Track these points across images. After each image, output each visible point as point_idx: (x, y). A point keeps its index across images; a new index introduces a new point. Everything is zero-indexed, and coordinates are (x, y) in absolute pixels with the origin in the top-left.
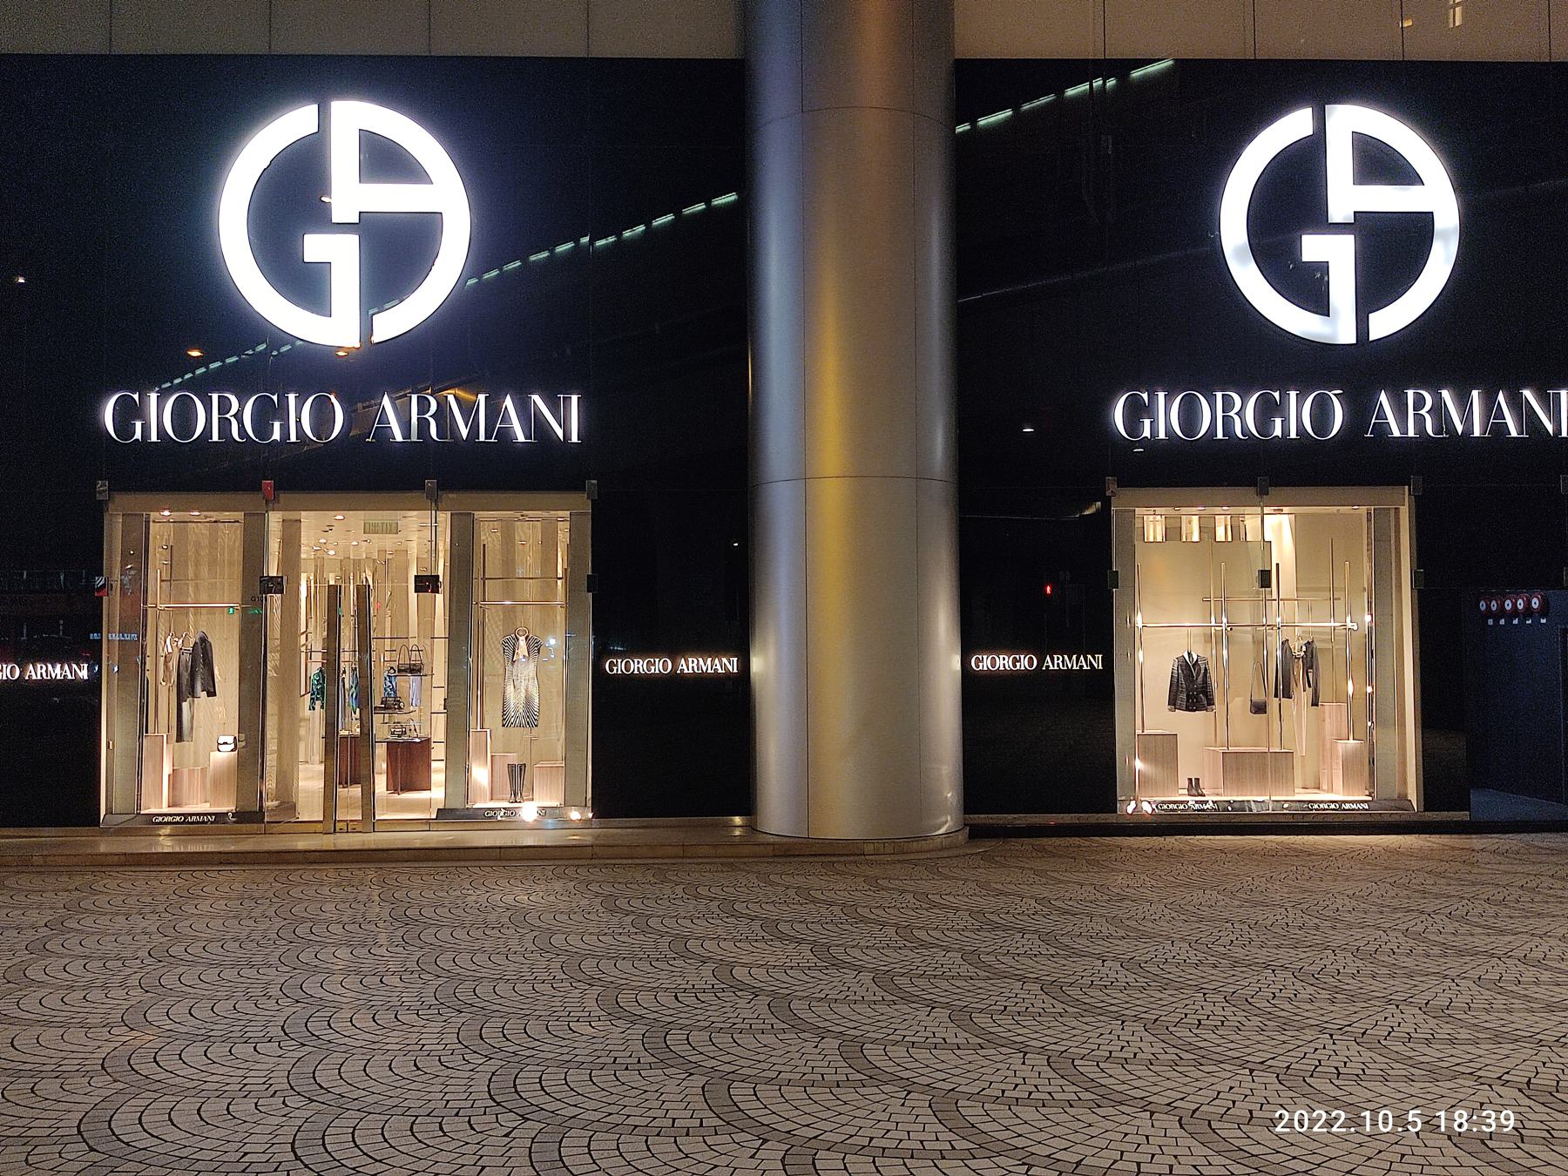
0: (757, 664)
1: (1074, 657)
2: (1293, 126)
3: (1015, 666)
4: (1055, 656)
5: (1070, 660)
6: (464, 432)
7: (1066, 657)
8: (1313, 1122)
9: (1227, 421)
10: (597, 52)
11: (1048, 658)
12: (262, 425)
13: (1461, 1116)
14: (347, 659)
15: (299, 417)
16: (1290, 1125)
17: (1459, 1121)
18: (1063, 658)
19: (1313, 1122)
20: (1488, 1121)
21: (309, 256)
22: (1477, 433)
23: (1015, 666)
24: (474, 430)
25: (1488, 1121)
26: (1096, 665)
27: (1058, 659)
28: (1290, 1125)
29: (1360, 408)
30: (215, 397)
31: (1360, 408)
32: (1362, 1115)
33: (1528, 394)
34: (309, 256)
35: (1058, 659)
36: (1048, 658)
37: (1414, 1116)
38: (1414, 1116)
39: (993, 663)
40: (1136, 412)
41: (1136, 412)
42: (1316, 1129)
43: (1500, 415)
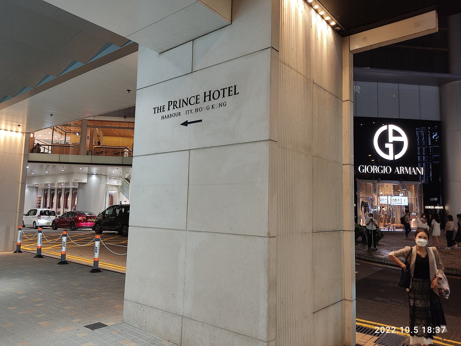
1: (410, 168)
2: (384, 128)
3: (380, 171)
4: (401, 167)
5: (408, 169)
7: (406, 168)
9: (375, 170)
10: (422, 118)
11: (397, 168)
13: (429, 328)
14: (48, 199)
15: (385, 170)
17: (430, 330)
20: (437, 330)
21: (386, 147)
22: (410, 174)
23: (380, 171)
24: (421, 174)
25: (437, 330)
26: (420, 173)
27: (402, 169)
29: (394, 169)
31: (394, 169)
33: (417, 168)
34: (386, 147)
35: (402, 169)
36: (397, 168)
37: (416, 328)
38: (416, 328)
39: (370, 169)
40: (362, 168)
41: (362, 168)
43: (413, 171)
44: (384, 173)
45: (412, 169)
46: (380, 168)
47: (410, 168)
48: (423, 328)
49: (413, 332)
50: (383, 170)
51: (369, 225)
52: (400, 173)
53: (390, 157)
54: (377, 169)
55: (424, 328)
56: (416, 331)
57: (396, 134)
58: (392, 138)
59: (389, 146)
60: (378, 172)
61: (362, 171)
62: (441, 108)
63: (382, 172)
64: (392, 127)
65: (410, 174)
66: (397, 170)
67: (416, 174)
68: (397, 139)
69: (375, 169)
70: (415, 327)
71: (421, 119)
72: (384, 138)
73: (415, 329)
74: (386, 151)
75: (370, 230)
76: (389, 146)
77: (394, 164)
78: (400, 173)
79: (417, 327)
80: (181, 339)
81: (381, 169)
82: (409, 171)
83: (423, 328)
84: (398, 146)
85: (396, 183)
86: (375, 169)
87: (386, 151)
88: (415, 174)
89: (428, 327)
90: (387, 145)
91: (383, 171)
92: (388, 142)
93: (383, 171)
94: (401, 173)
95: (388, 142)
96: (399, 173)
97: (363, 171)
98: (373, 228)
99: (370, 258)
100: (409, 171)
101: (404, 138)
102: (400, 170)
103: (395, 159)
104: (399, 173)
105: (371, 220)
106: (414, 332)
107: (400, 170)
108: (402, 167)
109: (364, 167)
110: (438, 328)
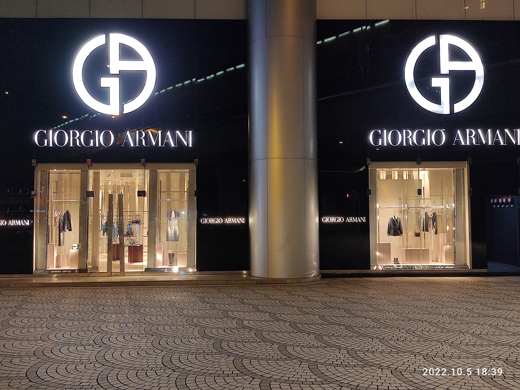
0: (251, 220)
1: (356, 218)
3: (337, 221)
4: (350, 218)
5: (355, 219)
6: (154, 143)
7: (353, 218)
8: (435, 372)
9: (407, 140)
10: (198, 17)
11: (348, 218)
12: (87, 141)
13: (484, 370)
14: (115, 218)
15: (99, 138)
16: (428, 373)
17: (484, 372)
18: (353, 218)
19: (435, 372)
20: (493, 372)
21: (103, 85)
22: (490, 144)
23: (337, 221)
25: (493, 372)
26: (363, 221)
27: (351, 218)
28: (428, 373)
29: (451, 135)
30: (71, 132)
31: (451, 135)
32: (452, 370)
33: (507, 131)
34: (103, 85)
35: (351, 218)
36: (348, 218)
37: (469, 370)
38: (469, 370)
39: (329, 220)
40: (377, 137)
41: (377, 137)
42: (436, 374)
43: (498, 138)
53: (444, 109)
80: (267, 284)
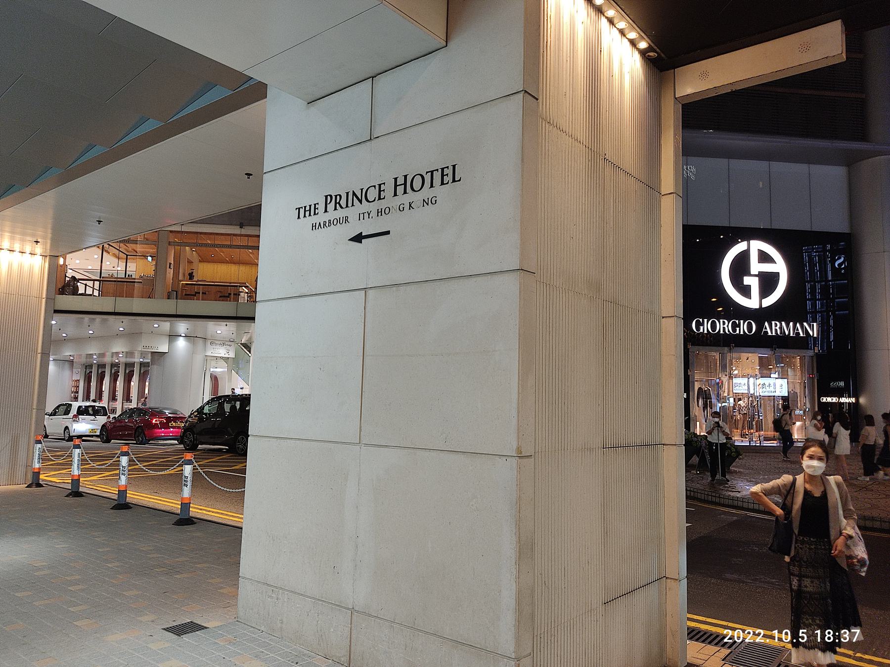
1: (791, 324)
2: (741, 247)
3: (734, 330)
4: (773, 322)
5: (788, 326)
7: (783, 323)
9: (724, 328)
10: (816, 228)
11: (766, 324)
13: (829, 633)
15: (743, 328)
17: (830, 636)
20: (844, 636)
21: (745, 283)
22: (791, 335)
23: (734, 330)
24: (813, 335)
25: (844, 636)
26: (811, 333)
27: (776, 325)
29: (760, 327)
31: (760, 327)
33: (805, 324)
34: (745, 283)
35: (776, 325)
36: (766, 324)
37: (803, 633)
38: (803, 633)
39: (714, 326)
40: (699, 324)
41: (699, 324)
43: (798, 330)
44: (742, 333)
45: (795, 326)
46: (734, 323)
47: (791, 324)
48: (816, 632)
49: (798, 641)
50: (740, 327)
51: (713, 433)
52: (772, 333)
53: (752, 303)
54: (728, 326)
55: (819, 632)
56: (803, 638)
57: (764, 257)
58: (756, 267)
59: (751, 282)
60: (730, 332)
61: (698, 329)
62: (850, 208)
63: (738, 332)
64: (757, 246)
65: (791, 335)
66: (766, 328)
67: (803, 335)
68: (767, 268)
69: (724, 326)
70: (801, 631)
71: (813, 230)
72: (741, 267)
73: (801, 635)
74: (745, 291)
75: (714, 443)
76: (751, 282)
77: (761, 315)
78: (772, 333)
79: (805, 631)
80: (350, 654)
81: (735, 326)
82: (789, 329)
83: (816, 632)
84: (768, 282)
85: (765, 353)
86: (724, 326)
87: (745, 291)
88: (801, 335)
89: (826, 630)
90: (747, 280)
91: (740, 330)
92: (748, 274)
93: (740, 330)
94: (774, 334)
95: (748, 274)
96: (770, 334)
97: (701, 330)
98: (720, 439)
99: (715, 496)
100: (789, 329)
101: (780, 266)
102: (773, 328)
103: (763, 307)
104: (770, 334)
105: (716, 425)
106: (800, 640)
107: (773, 328)
108: (776, 322)
109: (703, 321)
110: (845, 633)
